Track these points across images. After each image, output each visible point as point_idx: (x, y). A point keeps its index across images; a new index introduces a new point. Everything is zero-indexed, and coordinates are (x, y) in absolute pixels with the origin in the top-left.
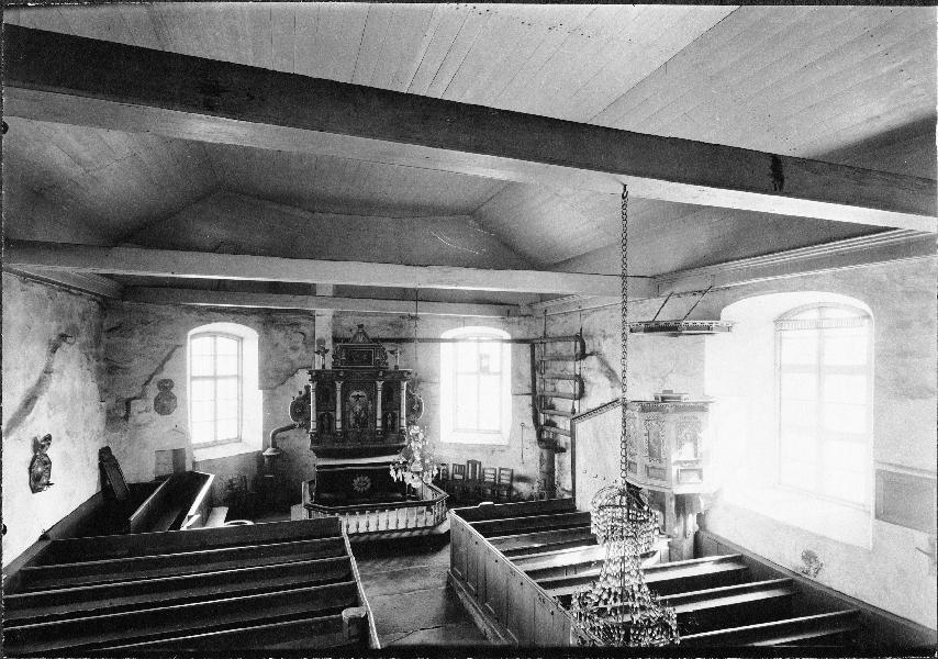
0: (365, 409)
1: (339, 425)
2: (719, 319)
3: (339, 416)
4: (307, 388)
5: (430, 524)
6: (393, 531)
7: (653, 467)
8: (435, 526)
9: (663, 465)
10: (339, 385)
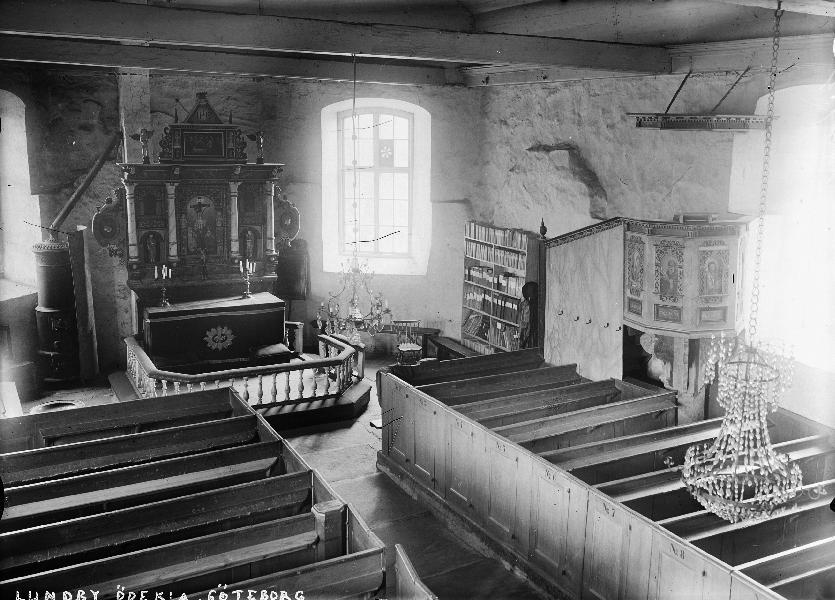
0: (211, 224)
1: (173, 250)
2: (753, 114)
3: (173, 237)
4: (121, 193)
5: (333, 391)
6: (283, 404)
7: (665, 307)
8: (338, 395)
9: (679, 305)
10: (171, 189)
